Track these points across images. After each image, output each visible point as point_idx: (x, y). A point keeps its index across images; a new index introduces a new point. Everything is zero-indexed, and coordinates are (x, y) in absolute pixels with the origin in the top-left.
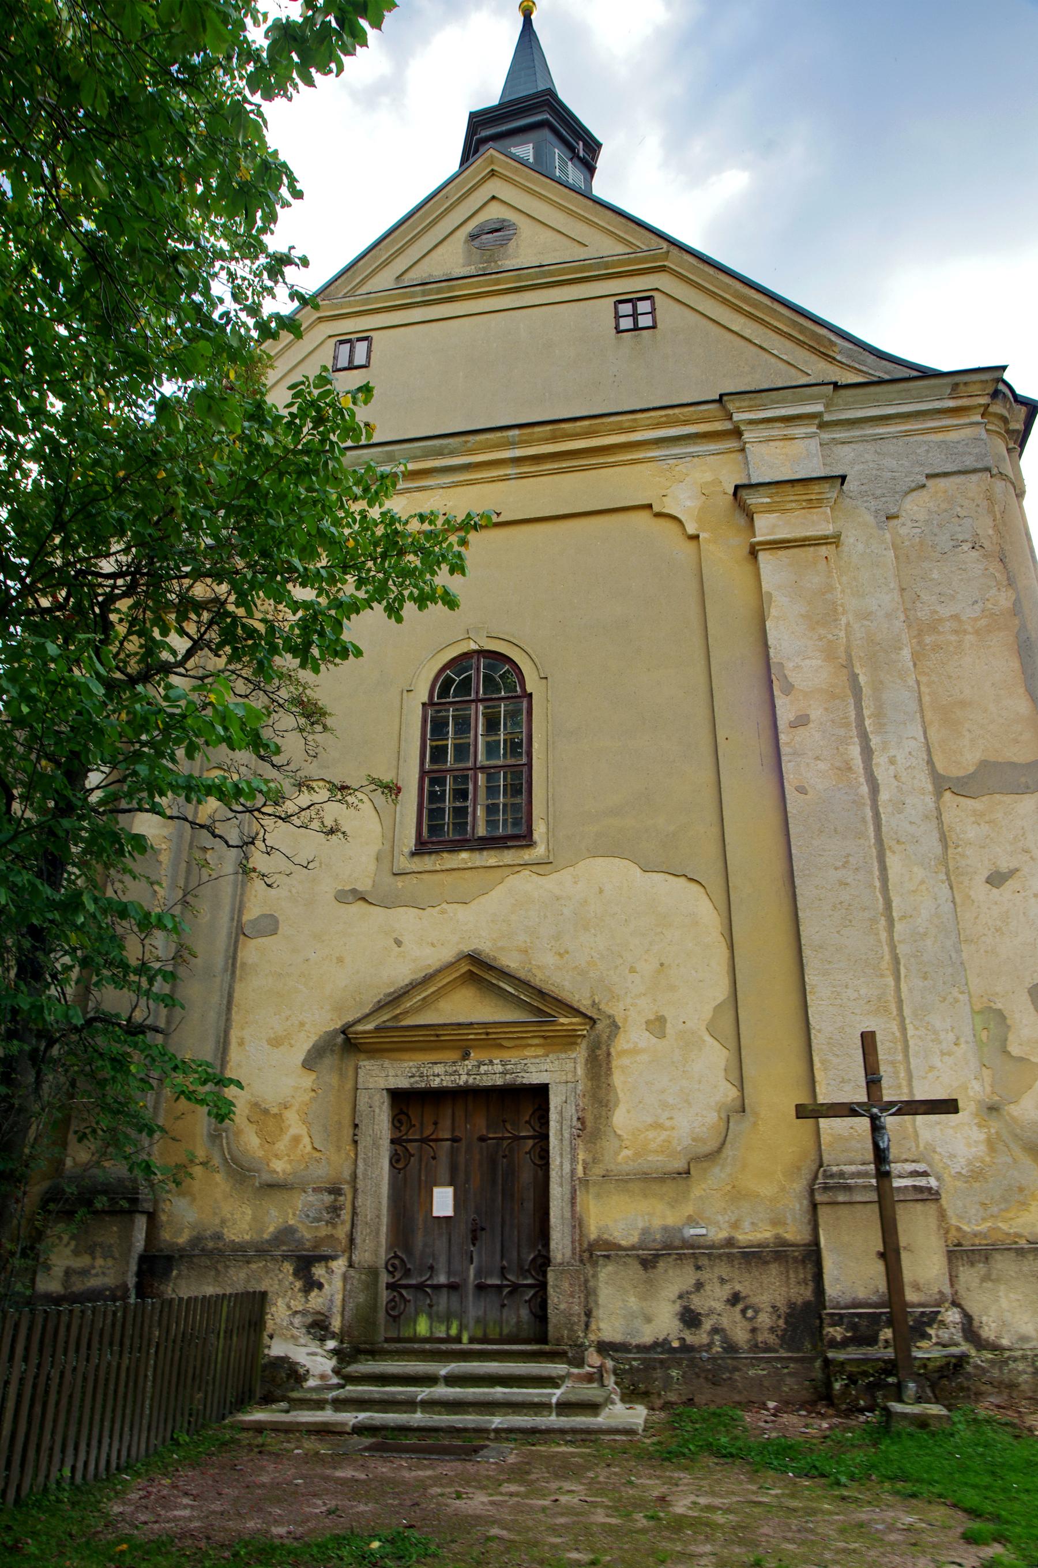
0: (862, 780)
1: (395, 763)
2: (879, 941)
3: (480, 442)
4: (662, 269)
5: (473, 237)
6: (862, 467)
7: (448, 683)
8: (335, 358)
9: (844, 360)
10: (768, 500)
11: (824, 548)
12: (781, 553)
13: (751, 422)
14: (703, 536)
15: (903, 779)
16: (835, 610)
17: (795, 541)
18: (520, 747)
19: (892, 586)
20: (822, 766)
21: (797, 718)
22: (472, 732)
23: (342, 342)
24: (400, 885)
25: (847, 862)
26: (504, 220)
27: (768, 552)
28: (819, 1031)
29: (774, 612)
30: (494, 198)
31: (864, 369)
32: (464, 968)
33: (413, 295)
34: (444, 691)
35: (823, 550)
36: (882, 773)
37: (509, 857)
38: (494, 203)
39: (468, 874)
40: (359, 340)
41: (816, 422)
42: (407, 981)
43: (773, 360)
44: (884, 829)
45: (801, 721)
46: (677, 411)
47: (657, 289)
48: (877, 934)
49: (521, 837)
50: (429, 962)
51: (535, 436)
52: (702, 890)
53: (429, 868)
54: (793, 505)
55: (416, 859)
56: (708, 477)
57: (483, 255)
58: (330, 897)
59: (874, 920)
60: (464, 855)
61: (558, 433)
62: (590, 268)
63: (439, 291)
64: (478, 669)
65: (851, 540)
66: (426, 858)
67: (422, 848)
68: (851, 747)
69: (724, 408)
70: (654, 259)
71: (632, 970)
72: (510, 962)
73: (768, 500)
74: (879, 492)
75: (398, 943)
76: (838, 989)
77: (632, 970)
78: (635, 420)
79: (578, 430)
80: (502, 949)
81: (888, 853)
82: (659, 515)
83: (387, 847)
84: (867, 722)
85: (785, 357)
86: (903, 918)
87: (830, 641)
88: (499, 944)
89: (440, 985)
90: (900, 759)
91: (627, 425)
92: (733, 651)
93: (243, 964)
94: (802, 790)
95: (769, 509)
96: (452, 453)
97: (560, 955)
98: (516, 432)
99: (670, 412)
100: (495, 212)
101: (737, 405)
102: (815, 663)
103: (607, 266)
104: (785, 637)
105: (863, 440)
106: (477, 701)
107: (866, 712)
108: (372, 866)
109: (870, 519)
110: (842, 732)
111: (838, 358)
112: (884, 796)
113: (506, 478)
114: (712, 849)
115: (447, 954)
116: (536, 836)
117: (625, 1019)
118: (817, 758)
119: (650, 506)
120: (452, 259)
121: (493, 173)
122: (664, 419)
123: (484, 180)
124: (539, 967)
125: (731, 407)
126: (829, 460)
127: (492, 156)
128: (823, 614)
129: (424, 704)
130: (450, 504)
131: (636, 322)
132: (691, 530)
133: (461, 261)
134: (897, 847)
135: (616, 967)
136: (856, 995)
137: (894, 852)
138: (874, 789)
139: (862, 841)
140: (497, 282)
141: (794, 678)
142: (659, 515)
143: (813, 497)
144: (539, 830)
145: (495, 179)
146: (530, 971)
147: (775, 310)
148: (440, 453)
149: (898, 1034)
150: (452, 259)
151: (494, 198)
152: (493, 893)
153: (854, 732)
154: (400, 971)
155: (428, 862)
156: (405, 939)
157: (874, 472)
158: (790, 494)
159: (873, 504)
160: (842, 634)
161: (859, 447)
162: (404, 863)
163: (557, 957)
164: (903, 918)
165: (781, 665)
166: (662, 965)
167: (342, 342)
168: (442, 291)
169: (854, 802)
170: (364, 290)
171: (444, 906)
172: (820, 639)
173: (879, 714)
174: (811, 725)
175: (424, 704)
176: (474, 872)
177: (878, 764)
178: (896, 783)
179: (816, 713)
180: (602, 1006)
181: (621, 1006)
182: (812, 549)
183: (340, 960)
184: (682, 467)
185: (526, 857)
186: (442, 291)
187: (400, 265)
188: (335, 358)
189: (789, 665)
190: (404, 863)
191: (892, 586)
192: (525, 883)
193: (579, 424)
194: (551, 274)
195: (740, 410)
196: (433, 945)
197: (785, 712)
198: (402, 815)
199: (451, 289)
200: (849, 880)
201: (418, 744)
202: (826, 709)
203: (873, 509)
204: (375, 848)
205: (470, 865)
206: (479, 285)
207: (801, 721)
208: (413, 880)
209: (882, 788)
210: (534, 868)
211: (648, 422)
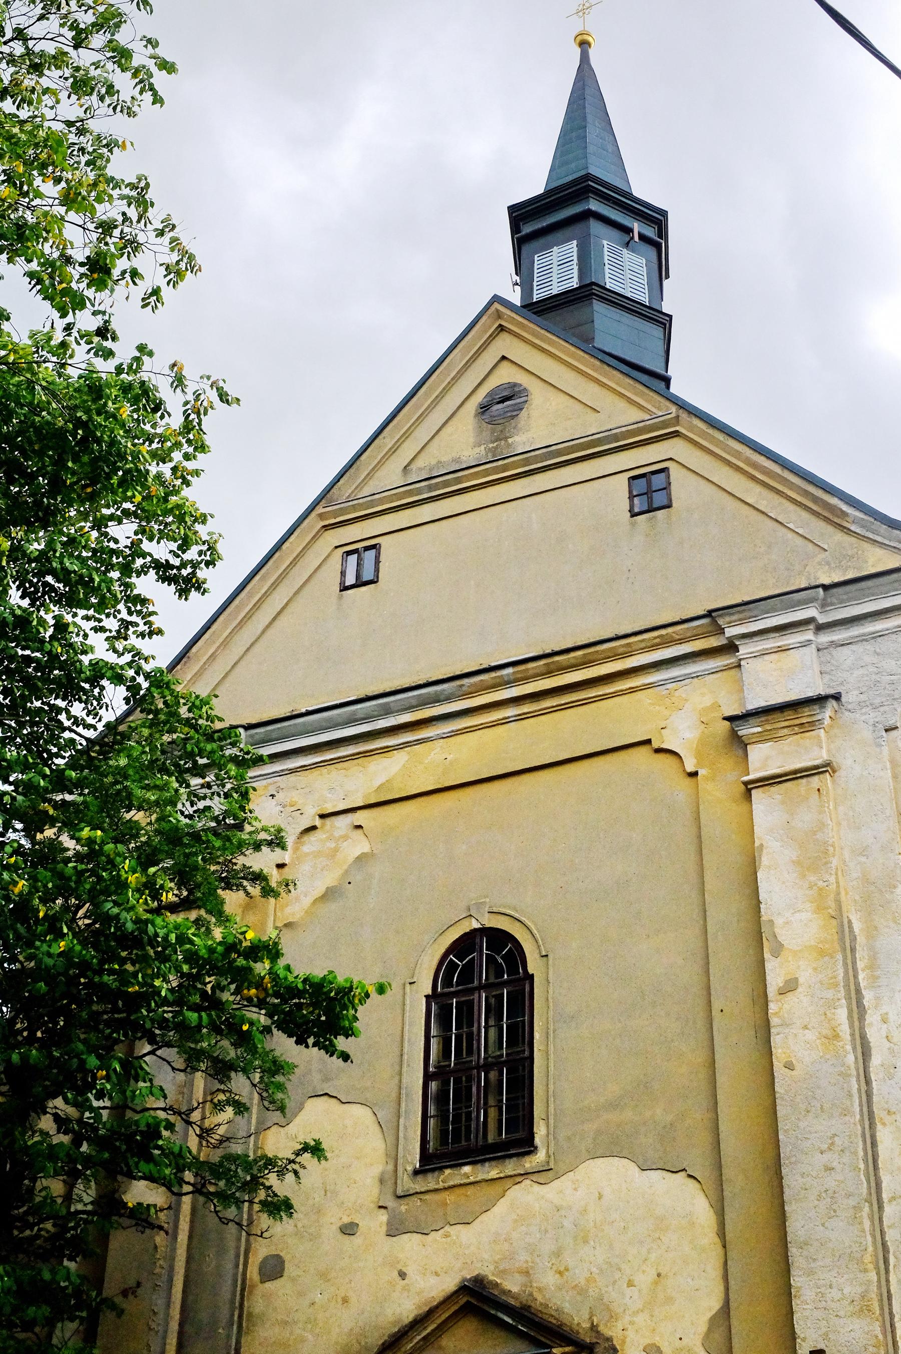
0: (849, 1048)
1: (397, 1068)
2: (863, 1231)
3: (475, 684)
4: (676, 434)
5: (484, 408)
6: (861, 671)
7: (452, 966)
8: (343, 573)
9: (858, 530)
10: (759, 729)
11: (816, 778)
12: (774, 789)
13: (744, 636)
14: (701, 772)
15: (895, 1040)
16: (826, 852)
17: (786, 774)
18: (521, 1035)
19: (888, 812)
20: (810, 1035)
21: (786, 982)
22: (476, 1025)
23: (349, 553)
24: (403, 1208)
25: (833, 1144)
26: (515, 385)
27: (760, 790)
28: (804, 1340)
29: (765, 860)
30: (504, 358)
31: (879, 539)
32: (463, 1300)
33: (419, 491)
34: (447, 982)
35: (815, 781)
36: (874, 1035)
37: (510, 1167)
38: (505, 364)
39: (470, 1191)
40: (367, 549)
41: (812, 627)
42: (411, 1319)
43: (790, 535)
44: (875, 1099)
45: (791, 986)
46: (670, 630)
47: (671, 459)
48: (861, 1223)
49: (519, 1141)
50: (433, 1294)
51: (531, 672)
52: (697, 1185)
53: (432, 1186)
54: (786, 731)
55: (420, 1178)
56: (708, 701)
57: (493, 431)
58: (335, 1228)
59: (857, 1208)
60: (467, 1169)
61: (552, 667)
62: (599, 442)
63: (446, 484)
64: (481, 950)
65: (849, 762)
66: (430, 1176)
67: (430, 1162)
68: (839, 1011)
69: (714, 622)
70: (665, 424)
71: (630, 1284)
72: (512, 1285)
73: (759, 729)
74: (877, 701)
75: (402, 1275)
76: (823, 1290)
77: (630, 1284)
78: (629, 645)
79: (573, 661)
80: (504, 1272)
81: (879, 1127)
82: (658, 751)
83: (390, 1167)
84: (861, 976)
85: (800, 531)
86: (892, 1199)
87: (821, 889)
88: (501, 1268)
89: (439, 1321)
90: (892, 1017)
91: (621, 650)
92: (725, 912)
93: (250, 1314)
94: (789, 1066)
95: (762, 739)
96: (449, 699)
97: (560, 1273)
98: (510, 670)
99: (663, 632)
100: (505, 375)
101: (728, 619)
102: (804, 916)
103: (616, 438)
104: (778, 891)
105: (863, 639)
106: (480, 988)
107: (860, 965)
108: (376, 1191)
109: (867, 734)
110: (830, 994)
111: (853, 528)
112: (876, 1061)
113: (505, 721)
114: (704, 1138)
115: (450, 1284)
116: (538, 1141)
117: (624, 1342)
118: (806, 1027)
119: (649, 742)
120: (461, 441)
121: (502, 328)
122: (658, 640)
123: (492, 337)
124: (540, 1289)
125: (721, 622)
126: (827, 668)
127: (497, 310)
128: (814, 858)
129: (427, 997)
130: (450, 757)
131: (650, 501)
132: (690, 768)
133: (472, 440)
134: (888, 1119)
135: (615, 1282)
136: (840, 1295)
137: (884, 1124)
138: (865, 1053)
139: (847, 1118)
140: (505, 468)
141: (783, 936)
142: (658, 751)
143: (804, 720)
144: (540, 1131)
145: (504, 336)
146: (531, 1294)
147: (786, 479)
148: (436, 700)
149: (881, 1337)
150: (461, 441)
151: (504, 358)
152: (495, 1210)
153: (842, 993)
154: (404, 1307)
155: (431, 1182)
156: (408, 1270)
157: (874, 677)
158: (780, 722)
159: (873, 716)
160: (832, 879)
161: (858, 648)
162: (407, 1183)
163: (558, 1276)
164: (892, 1199)
165: (771, 922)
166: (659, 1275)
167: (349, 553)
168: (443, 485)
169: (840, 1074)
170: (366, 491)
171: (447, 1228)
172: (811, 888)
173: (872, 966)
174: (800, 990)
175: (427, 997)
176: (477, 1187)
177: (871, 1024)
178: (888, 1045)
179: (805, 976)
180: (601, 1328)
181: (620, 1326)
182: (804, 781)
183: (345, 1300)
184: (683, 691)
185: (527, 1165)
186: (443, 485)
187: (408, 451)
188: (343, 573)
189: (779, 921)
190: (407, 1183)
191: (888, 812)
192: (525, 1195)
193: (572, 655)
194: (559, 453)
195: (731, 625)
196: (437, 1274)
197: (775, 979)
198: (406, 1128)
199: (459, 480)
200: (835, 1164)
201: (422, 1042)
202: (815, 969)
203: (871, 722)
204: (377, 1169)
205: (472, 1179)
206: (487, 473)
207: (791, 986)
208: (415, 1201)
209: (874, 1052)
210: (535, 1177)
211: (643, 645)
